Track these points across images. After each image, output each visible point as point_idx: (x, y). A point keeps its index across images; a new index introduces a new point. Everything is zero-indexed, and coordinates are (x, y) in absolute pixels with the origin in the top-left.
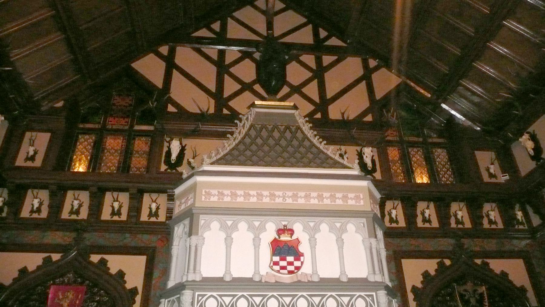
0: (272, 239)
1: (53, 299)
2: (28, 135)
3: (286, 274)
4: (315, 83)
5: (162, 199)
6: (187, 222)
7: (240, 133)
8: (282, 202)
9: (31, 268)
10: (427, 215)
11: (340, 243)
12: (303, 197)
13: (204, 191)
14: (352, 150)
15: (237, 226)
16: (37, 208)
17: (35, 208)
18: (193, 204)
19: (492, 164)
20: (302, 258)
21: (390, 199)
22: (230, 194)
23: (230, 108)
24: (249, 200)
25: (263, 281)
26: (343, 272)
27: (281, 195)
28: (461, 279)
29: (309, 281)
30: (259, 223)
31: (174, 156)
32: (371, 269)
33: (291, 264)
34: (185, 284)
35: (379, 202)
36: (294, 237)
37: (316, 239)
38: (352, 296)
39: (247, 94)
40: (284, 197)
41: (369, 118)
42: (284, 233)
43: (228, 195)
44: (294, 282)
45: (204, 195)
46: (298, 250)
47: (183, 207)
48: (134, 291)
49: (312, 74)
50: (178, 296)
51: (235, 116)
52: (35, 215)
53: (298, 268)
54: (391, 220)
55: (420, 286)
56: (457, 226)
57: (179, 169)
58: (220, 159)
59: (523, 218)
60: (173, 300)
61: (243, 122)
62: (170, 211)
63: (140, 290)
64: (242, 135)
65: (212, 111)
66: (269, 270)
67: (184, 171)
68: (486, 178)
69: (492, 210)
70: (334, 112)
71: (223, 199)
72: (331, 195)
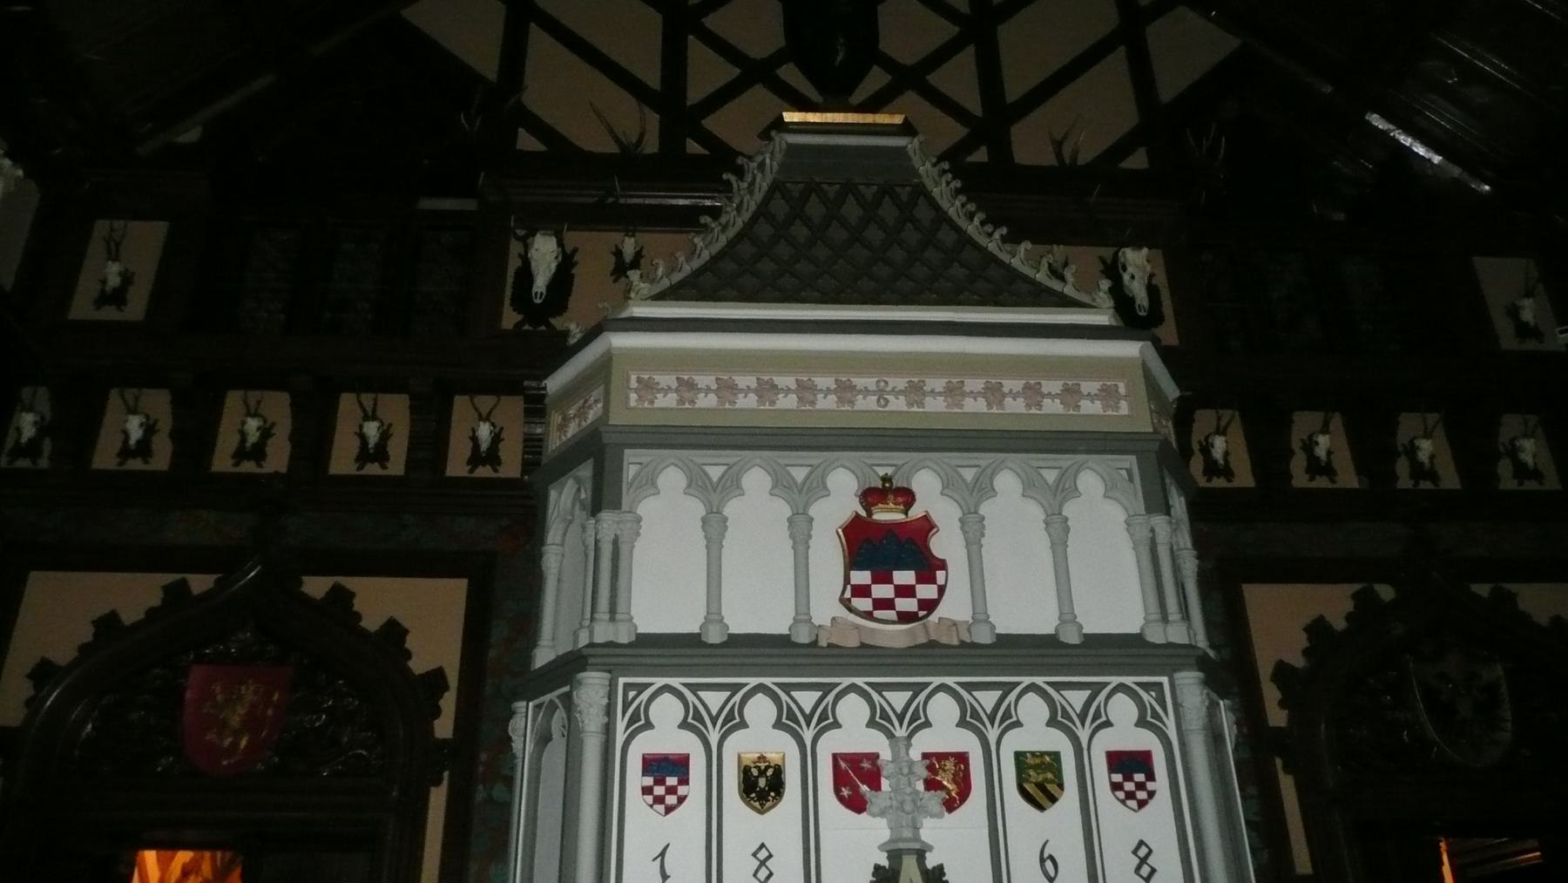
0: (845, 516)
2: (101, 227)
3: (893, 622)
4: (968, 56)
5: (511, 409)
6: (586, 471)
7: (739, 209)
8: (875, 407)
9: (130, 616)
10: (1321, 452)
11: (1058, 529)
12: (940, 394)
13: (633, 378)
14: (1087, 257)
15: (738, 480)
16: (138, 442)
17: (132, 441)
19: (1529, 294)
20: (940, 575)
21: (1206, 405)
22: (714, 387)
23: (707, 139)
24: (773, 403)
25: (823, 643)
27: (873, 387)
29: (963, 644)
30: (806, 471)
31: (540, 284)
33: (905, 591)
34: (585, 652)
35: (1173, 412)
36: (916, 512)
37: (983, 518)
38: (1096, 689)
39: (759, 95)
40: (881, 393)
41: (1138, 161)
42: (883, 500)
43: (708, 390)
44: (916, 647)
45: (636, 391)
46: (929, 550)
47: (572, 429)
48: (436, 679)
49: (957, 29)
50: (566, 689)
51: (720, 164)
52: (135, 464)
54: (1212, 468)
55: (1299, 662)
56: (1417, 484)
57: (557, 323)
58: (682, 284)
60: (551, 701)
61: (749, 178)
62: (533, 445)
63: (453, 679)
64: (746, 216)
65: (651, 146)
66: (842, 612)
67: (572, 327)
68: (1508, 341)
69: (1526, 436)
70: (1031, 145)
71: (692, 402)
72: (1027, 387)
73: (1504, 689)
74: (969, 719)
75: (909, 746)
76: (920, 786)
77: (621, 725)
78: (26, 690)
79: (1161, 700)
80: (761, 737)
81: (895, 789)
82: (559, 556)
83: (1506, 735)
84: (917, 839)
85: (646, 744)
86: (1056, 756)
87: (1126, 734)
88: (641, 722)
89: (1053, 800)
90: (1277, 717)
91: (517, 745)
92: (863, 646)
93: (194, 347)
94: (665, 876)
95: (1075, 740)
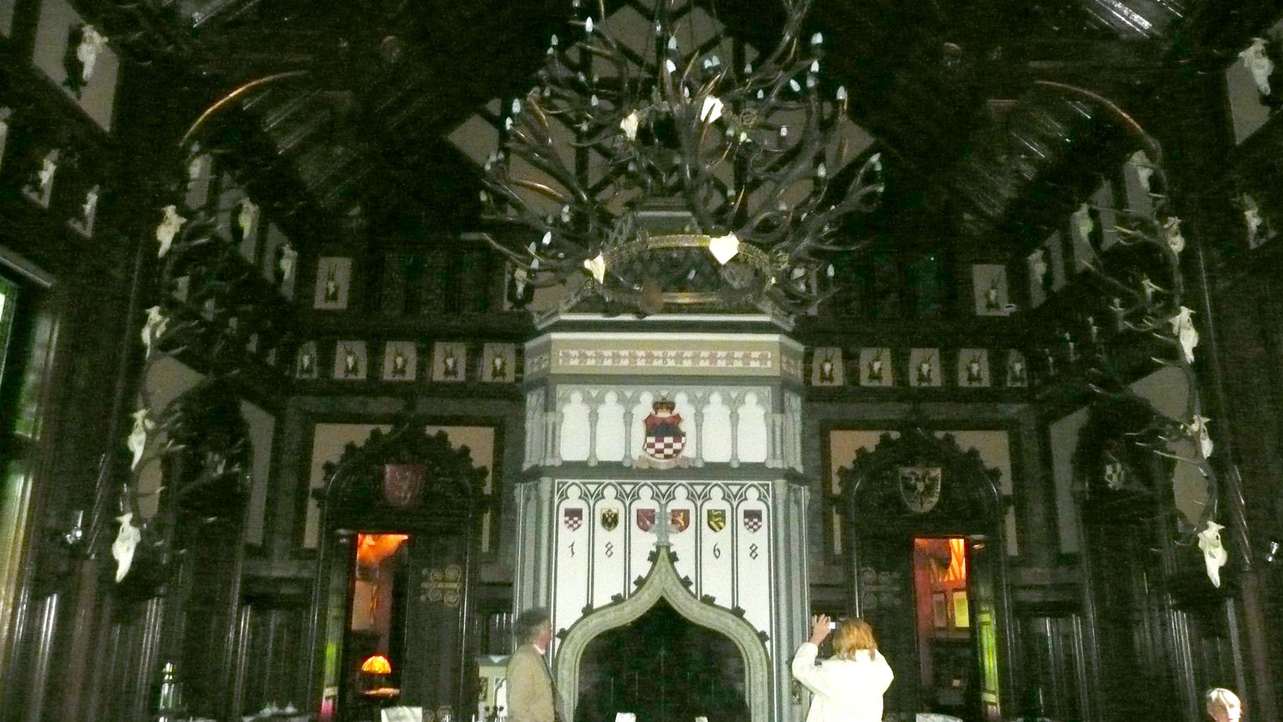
5: (509, 349)
9: (360, 443)
18: (549, 368)
26: (735, 456)
28: (910, 460)
33: (669, 446)
40: (664, 359)
59: (1025, 373)
66: (643, 453)
74: (691, 497)
76: (670, 522)
79: (767, 491)
80: (610, 502)
82: (533, 422)
83: (935, 500)
85: (566, 505)
86: (724, 511)
87: (752, 503)
88: (564, 496)
90: (836, 490)
91: (517, 500)
92: (650, 468)
93: (369, 322)
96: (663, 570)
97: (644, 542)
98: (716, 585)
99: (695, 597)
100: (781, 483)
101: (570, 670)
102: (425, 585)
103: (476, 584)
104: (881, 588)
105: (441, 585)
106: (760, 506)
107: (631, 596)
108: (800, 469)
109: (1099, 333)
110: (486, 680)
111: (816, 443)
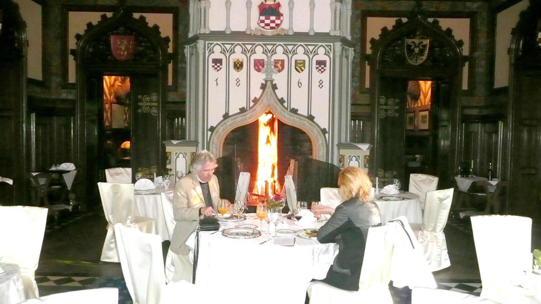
1: (114, 44)
9: (95, 23)
20: (282, 18)
26: (312, 28)
28: (411, 34)
29: (285, 35)
32: (333, 26)
33: (273, 22)
53: (278, 25)
63: (171, 38)
66: (257, 26)
73: (428, 47)
75: (271, 58)
76: (273, 67)
77: (207, 52)
78: (75, 41)
80: (238, 55)
81: (267, 67)
83: (424, 58)
84: (271, 78)
85: (213, 56)
86: (304, 61)
87: (321, 56)
88: (212, 52)
89: (302, 71)
90: (369, 51)
91: (186, 55)
94: (217, 84)
95: (288, 57)
96: (269, 93)
97: (258, 78)
98: (299, 102)
99: (287, 109)
100: (338, 46)
101: (216, 149)
102: (140, 104)
103: (165, 103)
104: (388, 107)
105: (149, 104)
106: (326, 58)
107: (250, 108)
108: (349, 38)
109: (112, 217)
110: (170, 153)
111: (359, 23)
